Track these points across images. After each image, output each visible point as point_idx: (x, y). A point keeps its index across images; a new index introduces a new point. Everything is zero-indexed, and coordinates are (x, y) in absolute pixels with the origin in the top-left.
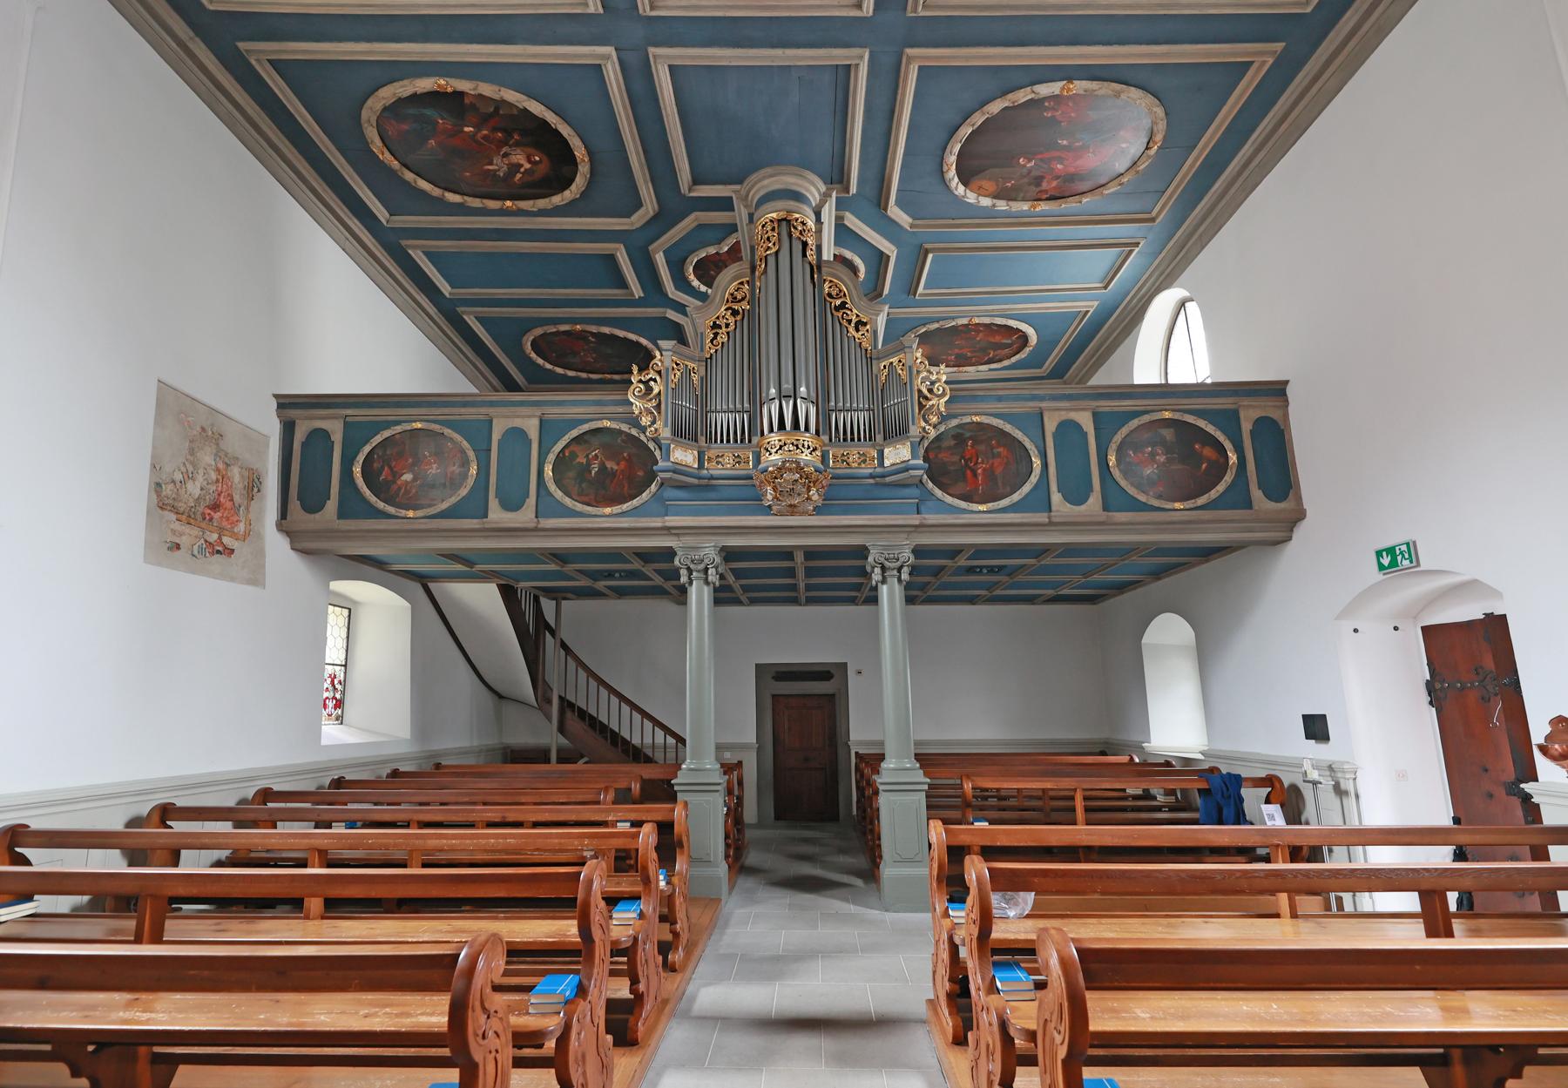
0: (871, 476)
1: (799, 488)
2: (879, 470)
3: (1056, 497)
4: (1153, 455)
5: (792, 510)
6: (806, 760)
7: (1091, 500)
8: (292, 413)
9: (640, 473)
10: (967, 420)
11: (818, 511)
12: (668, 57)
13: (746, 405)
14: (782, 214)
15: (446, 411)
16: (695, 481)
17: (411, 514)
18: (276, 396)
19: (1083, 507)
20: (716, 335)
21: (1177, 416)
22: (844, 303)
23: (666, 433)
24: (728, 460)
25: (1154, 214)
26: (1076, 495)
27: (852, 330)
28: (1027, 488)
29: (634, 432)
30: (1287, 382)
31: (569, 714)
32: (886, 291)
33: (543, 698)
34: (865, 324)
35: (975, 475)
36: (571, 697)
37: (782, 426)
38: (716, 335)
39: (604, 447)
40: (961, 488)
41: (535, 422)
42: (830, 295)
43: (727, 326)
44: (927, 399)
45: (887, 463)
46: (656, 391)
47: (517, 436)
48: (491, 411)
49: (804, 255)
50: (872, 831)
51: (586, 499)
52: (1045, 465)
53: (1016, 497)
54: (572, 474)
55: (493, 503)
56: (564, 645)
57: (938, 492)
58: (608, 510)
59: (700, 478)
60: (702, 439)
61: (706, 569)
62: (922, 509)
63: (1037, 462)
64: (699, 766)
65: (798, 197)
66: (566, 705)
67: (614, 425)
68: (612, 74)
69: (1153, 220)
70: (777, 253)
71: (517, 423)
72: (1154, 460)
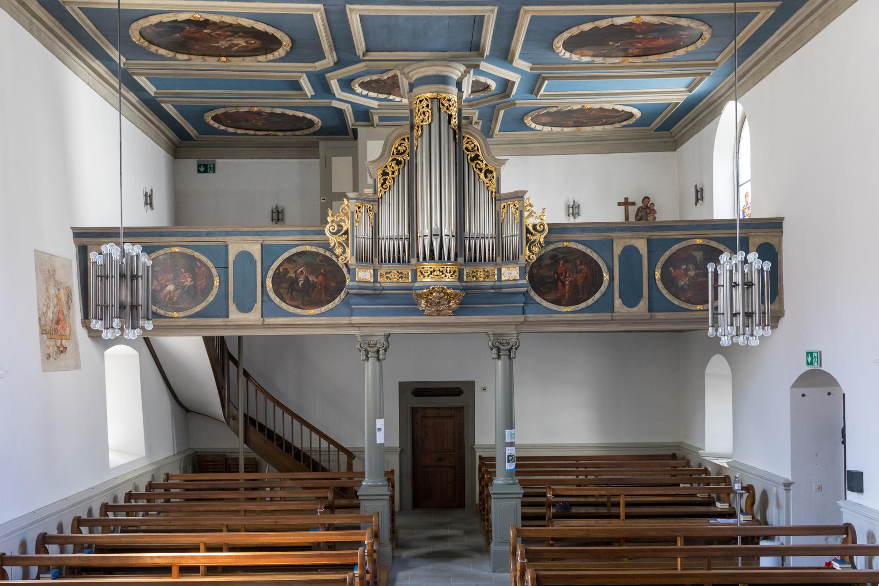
0: (492, 288)
1: (442, 302)
2: (498, 283)
3: (618, 302)
4: (687, 270)
5: (439, 313)
6: (440, 459)
7: (641, 304)
8: (85, 241)
9: (333, 284)
10: (560, 245)
11: (456, 312)
12: (359, 10)
13: (406, 233)
14: (435, 95)
15: (196, 239)
16: (372, 292)
17: (175, 314)
18: (72, 228)
19: (635, 309)
20: (385, 180)
21: (706, 242)
22: (477, 156)
23: (352, 261)
24: (394, 276)
25: (717, 60)
26: (631, 300)
27: (482, 176)
28: (598, 295)
29: (328, 254)
30: (783, 219)
31: (251, 429)
32: (514, 92)
33: (230, 418)
34: (491, 172)
35: (564, 285)
36: (252, 414)
37: (432, 258)
38: (385, 180)
39: (308, 265)
40: (552, 296)
41: (258, 247)
42: (467, 149)
43: (393, 173)
44: (531, 234)
45: (503, 278)
46: (345, 228)
47: (245, 257)
48: (227, 239)
49: (449, 123)
50: (488, 520)
51: (296, 303)
52: (612, 278)
53: (590, 301)
54: (285, 285)
55: (232, 307)
56: (246, 374)
57: (538, 299)
58: (312, 312)
59: (375, 290)
60: (376, 260)
61: (378, 351)
62: (527, 310)
63: (606, 277)
64: (371, 484)
65: (443, 80)
66: (250, 421)
67: (314, 249)
68: (319, 20)
69: (717, 64)
70: (430, 124)
71: (246, 247)
72: (686, 275)
